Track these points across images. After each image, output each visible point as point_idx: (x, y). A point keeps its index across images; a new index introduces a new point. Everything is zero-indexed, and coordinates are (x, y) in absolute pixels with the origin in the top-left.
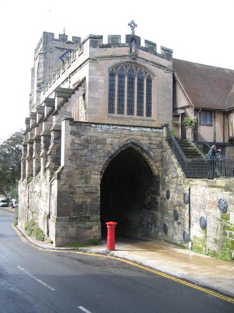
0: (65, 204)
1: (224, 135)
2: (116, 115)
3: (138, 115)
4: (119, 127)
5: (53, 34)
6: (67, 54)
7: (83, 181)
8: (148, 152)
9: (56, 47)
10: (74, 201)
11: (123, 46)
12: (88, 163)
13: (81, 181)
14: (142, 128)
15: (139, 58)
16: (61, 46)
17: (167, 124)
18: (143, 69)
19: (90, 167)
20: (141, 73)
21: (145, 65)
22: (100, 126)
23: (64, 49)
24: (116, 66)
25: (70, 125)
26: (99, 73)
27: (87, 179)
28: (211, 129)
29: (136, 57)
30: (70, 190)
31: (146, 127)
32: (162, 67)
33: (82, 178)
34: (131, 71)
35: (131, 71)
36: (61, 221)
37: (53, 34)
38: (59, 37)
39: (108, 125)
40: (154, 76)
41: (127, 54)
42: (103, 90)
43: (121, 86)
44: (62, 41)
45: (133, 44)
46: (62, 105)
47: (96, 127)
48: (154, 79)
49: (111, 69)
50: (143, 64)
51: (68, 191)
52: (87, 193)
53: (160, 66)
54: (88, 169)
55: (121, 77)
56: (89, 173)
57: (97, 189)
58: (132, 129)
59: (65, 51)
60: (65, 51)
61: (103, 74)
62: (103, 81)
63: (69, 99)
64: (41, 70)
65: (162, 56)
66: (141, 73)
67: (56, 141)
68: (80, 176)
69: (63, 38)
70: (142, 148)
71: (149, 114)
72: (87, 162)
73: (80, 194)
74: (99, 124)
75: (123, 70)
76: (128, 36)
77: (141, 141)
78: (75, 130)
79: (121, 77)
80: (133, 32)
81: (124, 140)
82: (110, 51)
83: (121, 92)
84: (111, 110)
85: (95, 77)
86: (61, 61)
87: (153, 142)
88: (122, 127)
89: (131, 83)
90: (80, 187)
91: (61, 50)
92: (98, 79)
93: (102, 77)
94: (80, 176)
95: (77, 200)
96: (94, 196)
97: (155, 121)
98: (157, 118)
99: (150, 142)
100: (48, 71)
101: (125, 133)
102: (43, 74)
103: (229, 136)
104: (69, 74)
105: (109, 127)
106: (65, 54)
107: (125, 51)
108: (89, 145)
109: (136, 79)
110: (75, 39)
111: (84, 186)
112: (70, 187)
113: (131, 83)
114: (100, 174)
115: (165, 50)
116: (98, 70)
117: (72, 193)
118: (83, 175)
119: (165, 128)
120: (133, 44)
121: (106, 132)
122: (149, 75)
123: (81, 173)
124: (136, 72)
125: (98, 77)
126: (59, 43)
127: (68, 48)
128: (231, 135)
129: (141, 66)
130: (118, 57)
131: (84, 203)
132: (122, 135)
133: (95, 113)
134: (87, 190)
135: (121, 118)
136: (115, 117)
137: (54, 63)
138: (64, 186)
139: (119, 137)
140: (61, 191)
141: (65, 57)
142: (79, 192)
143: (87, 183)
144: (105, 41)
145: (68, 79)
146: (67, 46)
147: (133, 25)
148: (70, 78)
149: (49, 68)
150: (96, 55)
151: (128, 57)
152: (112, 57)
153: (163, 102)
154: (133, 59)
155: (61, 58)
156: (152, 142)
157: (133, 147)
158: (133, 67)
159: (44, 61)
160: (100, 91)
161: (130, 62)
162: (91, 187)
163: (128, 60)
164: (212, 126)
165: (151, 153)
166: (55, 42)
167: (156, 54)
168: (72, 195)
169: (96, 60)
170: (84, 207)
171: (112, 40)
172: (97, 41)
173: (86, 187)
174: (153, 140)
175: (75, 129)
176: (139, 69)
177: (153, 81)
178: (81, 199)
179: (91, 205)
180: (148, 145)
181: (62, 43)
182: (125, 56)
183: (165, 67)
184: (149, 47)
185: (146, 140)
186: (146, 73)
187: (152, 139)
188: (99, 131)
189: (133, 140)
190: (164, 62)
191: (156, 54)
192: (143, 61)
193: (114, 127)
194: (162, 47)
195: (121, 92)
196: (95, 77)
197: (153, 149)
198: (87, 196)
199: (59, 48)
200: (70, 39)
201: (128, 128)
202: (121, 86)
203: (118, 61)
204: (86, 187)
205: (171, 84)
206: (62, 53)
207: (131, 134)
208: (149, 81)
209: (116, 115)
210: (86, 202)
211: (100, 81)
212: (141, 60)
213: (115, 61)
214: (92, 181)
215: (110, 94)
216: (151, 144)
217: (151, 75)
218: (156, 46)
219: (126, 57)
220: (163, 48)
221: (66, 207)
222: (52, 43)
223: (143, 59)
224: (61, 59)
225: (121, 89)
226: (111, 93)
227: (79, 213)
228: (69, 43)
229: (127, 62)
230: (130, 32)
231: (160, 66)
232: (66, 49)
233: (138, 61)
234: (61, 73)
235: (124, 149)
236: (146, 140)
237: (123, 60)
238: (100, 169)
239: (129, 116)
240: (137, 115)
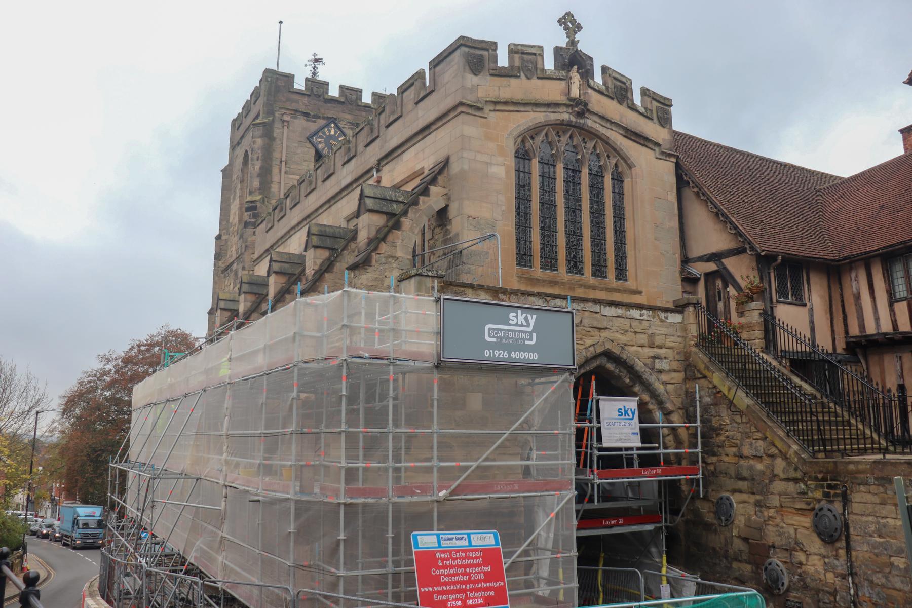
1: (833, 331)
6: (326, 130)
24: (534, 132)
28: (802, 312)
41: (563, 99)
42: (502, 198)
43: (548, 190)
46: (384, 239)
49: (520, 139)
50: (602, 130)
55: (548, 163)
59: (322, 122)
60: (322, 122)
63: (403, 219)
69: (316, 87)
71: (621, 272)
76: (558, 51)
80: (573, 43)
82: (517, 88)
83: (548, 205)
84: (523, 257)
86: (310, 146)
89: (572, 182)
93: (500, 159)
103: (847, 332)
104: (379, 157)
107: (553, 91)
113: (572, 182)
119: (691, 308)
122: (616, 165)
128: (854, 331)
141: (321, 137)
144: (503, 60)
147: (570, 24)
148: (378, 171)
149: (278, 163)
150: (482, 94)
151: (565, 109)
155: (309, 139)
161: (569, 124)
163: (566, 117)
164: (805, 305)
180: (649, 361)
182: (557, 105)
183: (657, 144)
186: (608, 157)
189: (609, 346)
191: (633, 108)
195: (548, 205)
200: (334, 92)
202: (548, 190)
206: (313, 127)
209: (537, 271)
213: (532, 115)
219: (561, 109)
224: (311, 142)
225: (546, 197)
226: (522, 207)
228: (333, 100)
230: (563, 41)
234: (276, 219)
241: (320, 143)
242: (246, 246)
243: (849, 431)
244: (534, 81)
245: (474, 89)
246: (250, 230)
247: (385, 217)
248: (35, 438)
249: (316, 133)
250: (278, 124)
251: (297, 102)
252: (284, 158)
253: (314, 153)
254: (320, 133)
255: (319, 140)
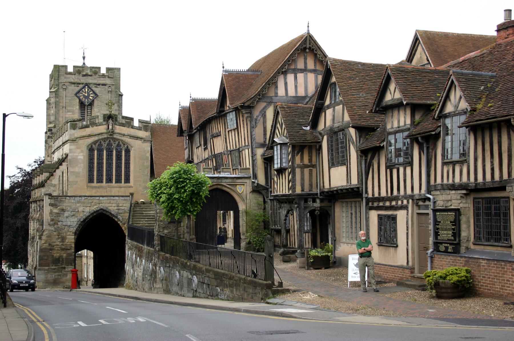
0: (46, 258)
2: (104, 184)
3: (125, 182)
4: (89, 198)
5: (66, 67)
6: (83, 90)
7: (59, 240)
8: (116, 216)
9: (70, 83)
10: (53, 255)
11: (101, 124)
12: (64, 226)
13: (58, 241)
14: (110, 197)
15: (116, 133)
16: (76, 81)
17: (132, 193)
18: (120, 142)
19: (65, 230)
20: (119, 145)
21: (122, 139)
22: (73, 198)
23: (79, 84)
24: (95, 142)
25: (49, 198)
26: (79, 150)
27: (63, 239)
29: (113, 132)
30: (49, 248)
31: (114, 196)
32: (139, 139)
33: (59, 238)
34: (109, 144)
35: (109, 144)
36: (42, 270)
37: (66, 67)
38: (74, 69)
39: (80, 196)
40: (132, 147)
41: (105, 131)
42: (82, 165)
44: (77, 74)
45: (110, 121)
46: (48, 179)
47: (70, 199)
48: (132, 150)
49: (90, 146)
50: (120, 138)
51: (48, 248)
52: (63, 249)
53: (137, 138)
54: (64, 231)
55: (100, 151)
56: (64, 234)
57: (72, 247)
58: (101, 198)
61: (82, 152)
62: (82, 157)
64: (52, 112)
65: (139, 129)
66: (119, 145)
67: (28, 213)
68: (57, 237)
70: (111, 213)
71: (127, 180)
72: (63, 226)
73: (58, 250)
74: (72, 196)
75: (102, 145)
77: (110, 208)
78: (53, 202)
79: (100, 151)
81: (95, 208)
83: (100, 164)
84: (91, 180)
85: (75, 154)
86: (76, 98)
87: (121, 208)
88: (92, 198)
90: (57, 245)
91: (76, 85)
92: (77, 156)
93: (82, 154)
94: (57, 237)
95: (55, 255)
96: (69, 252)
97: (132, 187)
98: (134, 185)
99: (118, 208)
100: (61, 111)
101: (95, 202)
102: (54, 117)
105: (81, 198)
106: (81, 90)
107: (102, 129)
108: (65, 213)
109: (114, 152)
110: (93, 70)
111: (61, 244)
112: (50, 244)
114: (74, 234)
115: (142, 123)
116: (78, 148)
117: (51, 250)
118: (60, 236)
119: (307, 148)
120: (110, 121)
121: (79, 202)
123: (58, 234)
124: (114, 146)
125: (77, 154)
126: (73, 76)
127: (85, 82)
129: (118, 139)
130: (96, 135)
131: (61, 257)
132: (92, 204)
133: (76, 185)
134: (63, 247)
135: (99, 187)
136: (94, 187)
137: (68, 101)
138: (44, 244)
139: (90, 205)
140: (42, 248)
142: (56, 249)
143: (63, 242)
145: (62, 146)
146: (84, 80)
151: (105, 134)
152: (90, 136)
153: (140, 170)
154: (111, 135)
155: (76, 94)
156: (120, 208)
157: (104, 212)
158: (111, 141)
159: (56, 101)
160: (79, 165)
161: (108, 138)
162: (66, 245)
163: (106, 136)
165: (119, 217)
166: (69, 76)
167: (133, 127)
168: (51, 251)
169: (76, 140)
170: (61, 260)
171: (90, 121)
172: (76, 124)
173: (62, 245)
174: (121, 206)
175: (53, 201)
176: (117, 143)
177: (131, 151)
178: (58, 254)
179: (66, 258)
181: (77, 76)
184: (126, 122)
185: (114, 207)
187: (120, 206)
188: (72, 202)
190: (142, 134)
191: (133, 127)
192: (120, 135)
193: (86, 198)
194: (139, 120)
195: (100, 164)
196: (75, 154)
197: (121, 213)
198: (63, 252)
199: (74, 83)
201: (98, 198)
203: (96, 138)
204: (62, 245)
205: (148, 152)
206: (77, 89)
207: (101, 202)
208: (128, 151)
209: (104, 184)
210: (63, 256)
211: (79, 157)
212: (118, 135)
214: (67, 241)
215: (90, 166)
216: (119, 209)
217: (129, 147)
218: (133, 120)
220: (140, 121)
221: (46, 260)
222: (65, 78)
223: (119, 134)
226: (91, 166)
227: (57, 265)
229: (105, 138)
231: (137, 138)
232: (82, 84)
233: (115, 136)
235: (95, 214)
236: (114, 207)
237: (101, 137)
238: (74, 231)
239: (107, 184)
240: (97, 182)
241: (81, 96)
242: (49, 146)
243: (468, 206)
244: (95, 127)
245: (74, 134)
246: (50, 140)
247: (49, 173)
248: (215, 279)
249: (78, 92)
250: (61, 90)
251: (69, 78)
252: (64, 106)
253: (78, 101)
254: (81, 92)
255: (80, 95)
